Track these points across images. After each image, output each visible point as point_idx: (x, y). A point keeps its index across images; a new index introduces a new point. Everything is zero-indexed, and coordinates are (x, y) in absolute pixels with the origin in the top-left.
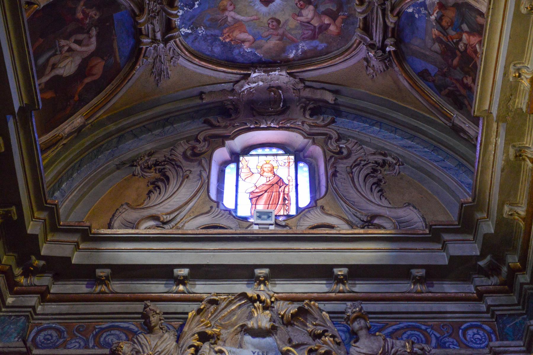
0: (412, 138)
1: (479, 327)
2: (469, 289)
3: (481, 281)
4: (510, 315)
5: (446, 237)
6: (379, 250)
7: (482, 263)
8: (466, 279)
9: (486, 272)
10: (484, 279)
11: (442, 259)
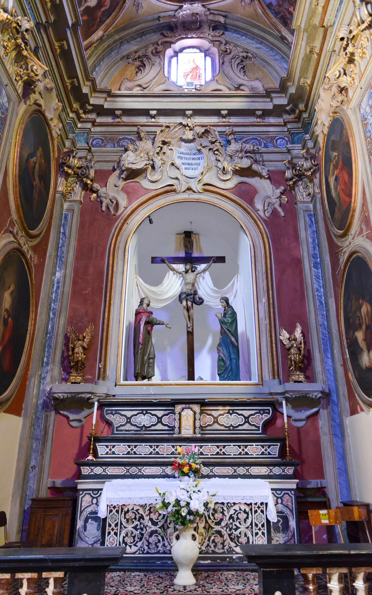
0: (261, 43)
1: (283, 138)
2: (280, 121)
3: (286, 117)
4: (297, 133)
5: (273, 95)
6: (248, 102)
7: (287, 108)
8: (280, 116)
9: (289, 113)
10: (288, 116)
11: (270, 106)
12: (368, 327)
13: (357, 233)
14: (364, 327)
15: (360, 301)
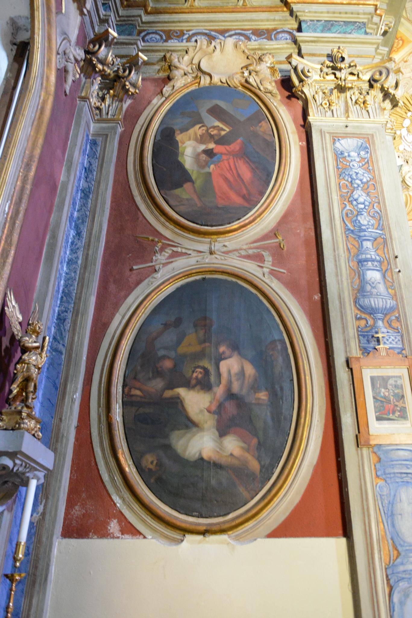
12: (230, 395)
13: (243, 253)
14: (220, 391)
15: (222, 349)
